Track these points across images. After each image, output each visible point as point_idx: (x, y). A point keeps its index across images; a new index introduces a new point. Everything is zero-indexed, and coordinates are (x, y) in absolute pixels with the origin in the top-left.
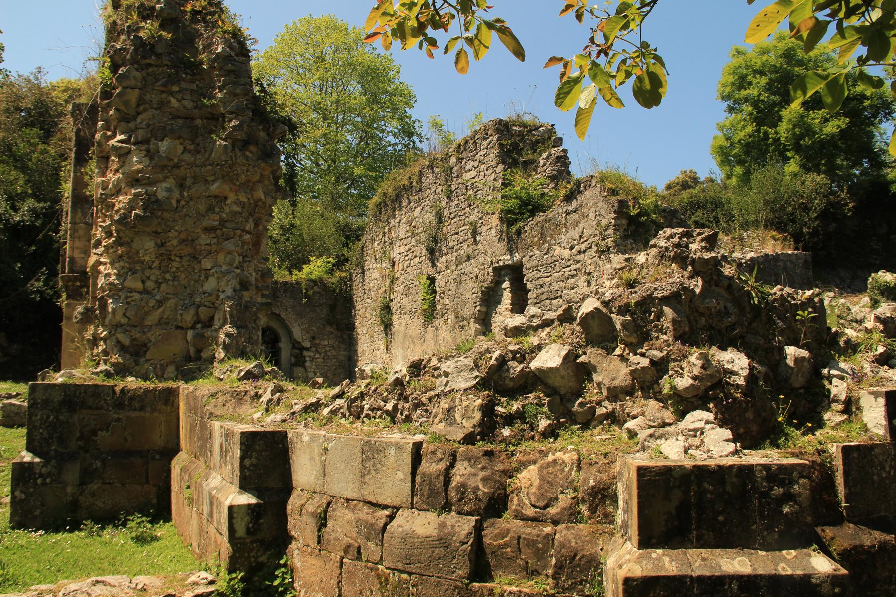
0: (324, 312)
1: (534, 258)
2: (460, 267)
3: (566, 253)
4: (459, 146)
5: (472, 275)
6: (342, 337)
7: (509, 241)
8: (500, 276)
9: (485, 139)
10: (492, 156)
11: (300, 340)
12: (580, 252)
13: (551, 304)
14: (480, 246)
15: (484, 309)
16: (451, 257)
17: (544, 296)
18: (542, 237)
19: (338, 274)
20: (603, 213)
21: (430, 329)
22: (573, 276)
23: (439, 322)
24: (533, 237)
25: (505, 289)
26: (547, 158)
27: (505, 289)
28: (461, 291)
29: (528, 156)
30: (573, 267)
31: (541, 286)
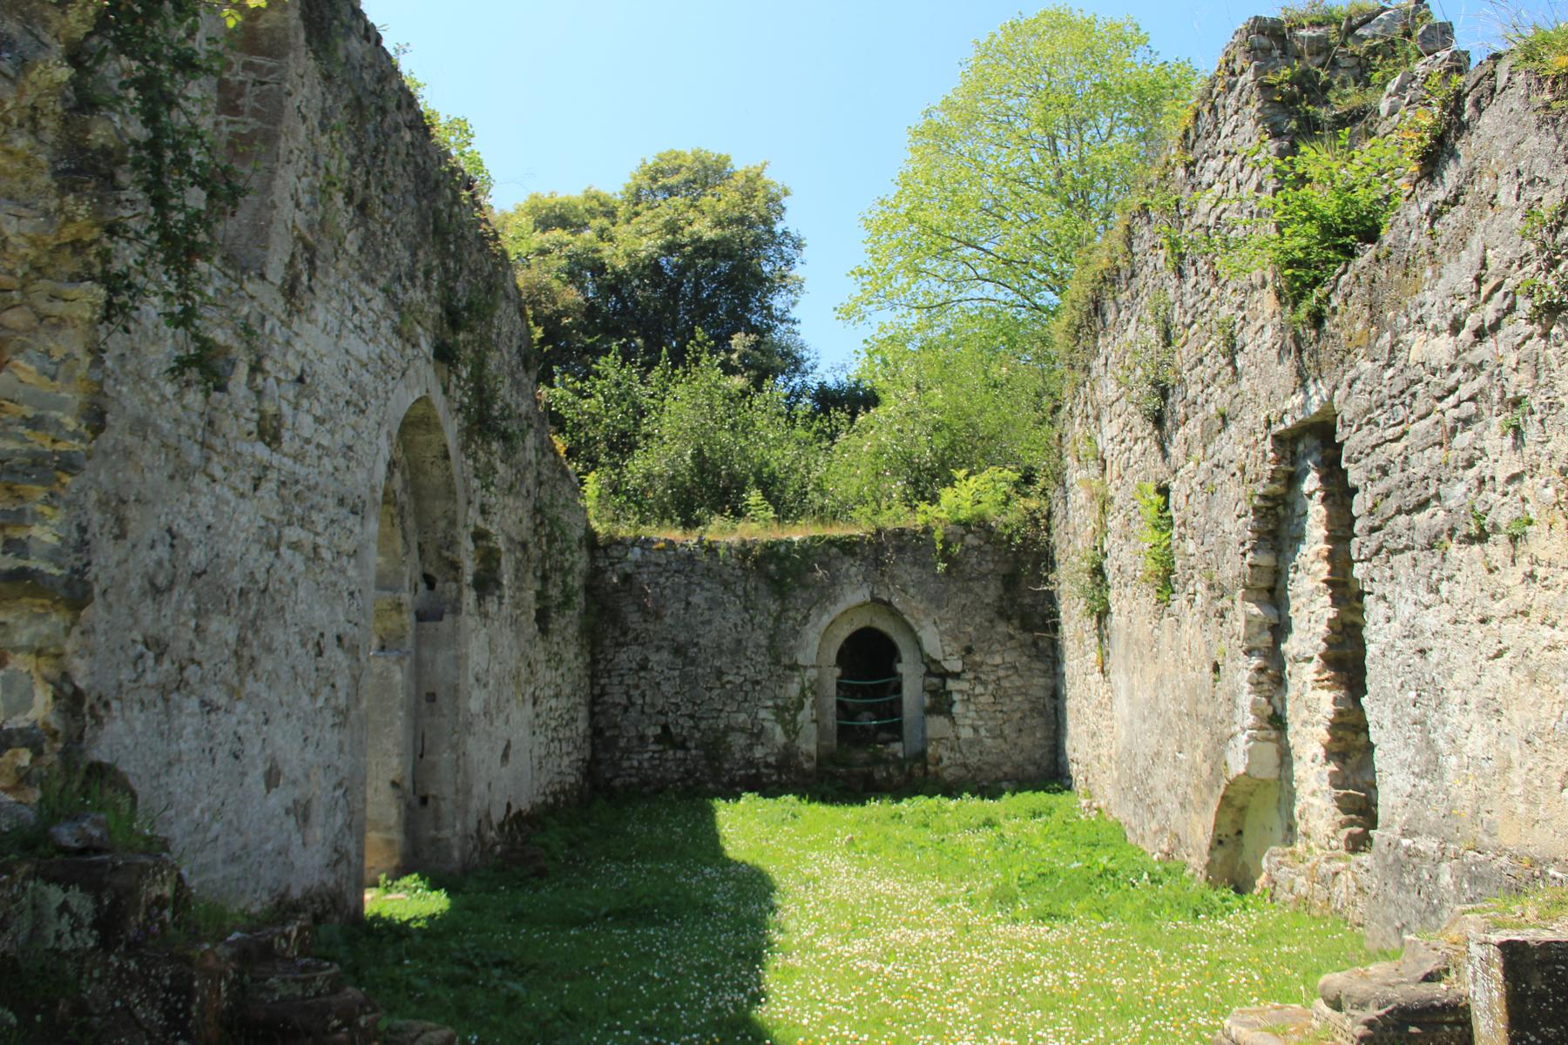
0: (992, 592)
1: (1358, 386)
2: (1210, 451)
3: (1442, 348)
4: (1186, 135)
5: (1233, 468)
6: (1035, 644)
8: (1294, 459)
9: (1231, 87)
10: (1249, 124)
11: (938, 656)
12: (1480, 334)
14: (1245, 384)
15: (1266, 560)
16: (1192, 429)
17: (1392, 504)
19: (1020, 504)
20: (1542, 169)
21: (1166, 620)
22: (1467, 422)
23: (1180, 601)
25: (1310, 496)
26: (1402, 88)
28: (1214, 513)
29: (1349, 98)
30: (1464, 392)
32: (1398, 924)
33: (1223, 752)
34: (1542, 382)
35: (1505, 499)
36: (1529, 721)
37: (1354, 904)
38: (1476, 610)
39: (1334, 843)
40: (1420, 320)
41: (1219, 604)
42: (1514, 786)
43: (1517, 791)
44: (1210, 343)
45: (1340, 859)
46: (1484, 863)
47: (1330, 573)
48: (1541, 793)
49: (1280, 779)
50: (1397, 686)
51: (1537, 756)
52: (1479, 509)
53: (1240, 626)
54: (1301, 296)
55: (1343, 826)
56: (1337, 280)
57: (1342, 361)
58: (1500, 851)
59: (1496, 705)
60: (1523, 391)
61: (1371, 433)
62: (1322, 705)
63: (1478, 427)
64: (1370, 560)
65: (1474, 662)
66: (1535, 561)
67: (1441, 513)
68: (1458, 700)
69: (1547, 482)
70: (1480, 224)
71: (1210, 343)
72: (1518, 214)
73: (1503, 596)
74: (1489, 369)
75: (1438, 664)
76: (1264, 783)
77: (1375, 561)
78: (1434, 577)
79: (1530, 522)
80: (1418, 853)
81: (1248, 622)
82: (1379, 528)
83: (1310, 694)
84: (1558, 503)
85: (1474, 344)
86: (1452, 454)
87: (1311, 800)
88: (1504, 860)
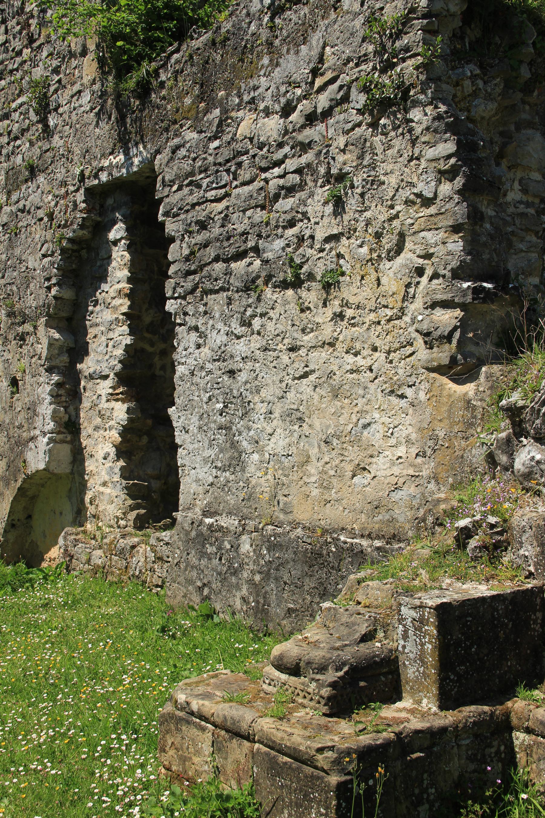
1: (183, 152)
2: (14, 197)
3: (272, 126)
5: (41, 213)
7: (121, 120)
12: (311, 119)
13: (228, 273)
14: (57, 141)
15: (68, 294)
17: (211, 252)
18: (206, 96)
24: (180, 97)
25: (115, 243)
27: (115, 243)
28: (17, 251)
30: (291, 164)
31: (203, 225)
32: (199, 584)
33: (22, 452)
34: (365, 163)
35: (321, 255)
36: (328, 427)
37: (152, 570)
38: (286, 341)
39: (122, 523)
40: (252, 101)
41: (20, 329)
42: (309, 476)
43: (313, 479)
44: (20, 101)
45: (131, 535)
46: (283, 534)
47: (130, 307)
48: (334, 481)
49: (72, 473)
50: (205, 399)
51: (334, 453)
52: (298, 261)
53: (42, 348)
54: (129, 69)
55: (132, 508)
56: (169, 57)
57: (167, 130)
58: (295, 525)
59: (299, 415)
60: (347, 169)
61: (191, 193)
62: (115, 414)
63: (302, 195)
64: (184, 298)
65: (281, 381)
66: (346, 304)
67: (258, 263)
68: (263, 410)
69: (363, 243)
70: (322, 24)
71: (20, 101)
72: (361, 19)
73: (312, 330)
74: (317, 148)
75: (246, 382)
76: (58, 477)
77: (190, 298)
78: (248, 313)
79: (343, 274)
80: (220, 529)
81: (50, 345)
82: (194, 272)
83: (104, 405)
84: (371, 260)
85: (303, 127)
86: (273, 215)
87: (102, 489)
88: (299, 531)
